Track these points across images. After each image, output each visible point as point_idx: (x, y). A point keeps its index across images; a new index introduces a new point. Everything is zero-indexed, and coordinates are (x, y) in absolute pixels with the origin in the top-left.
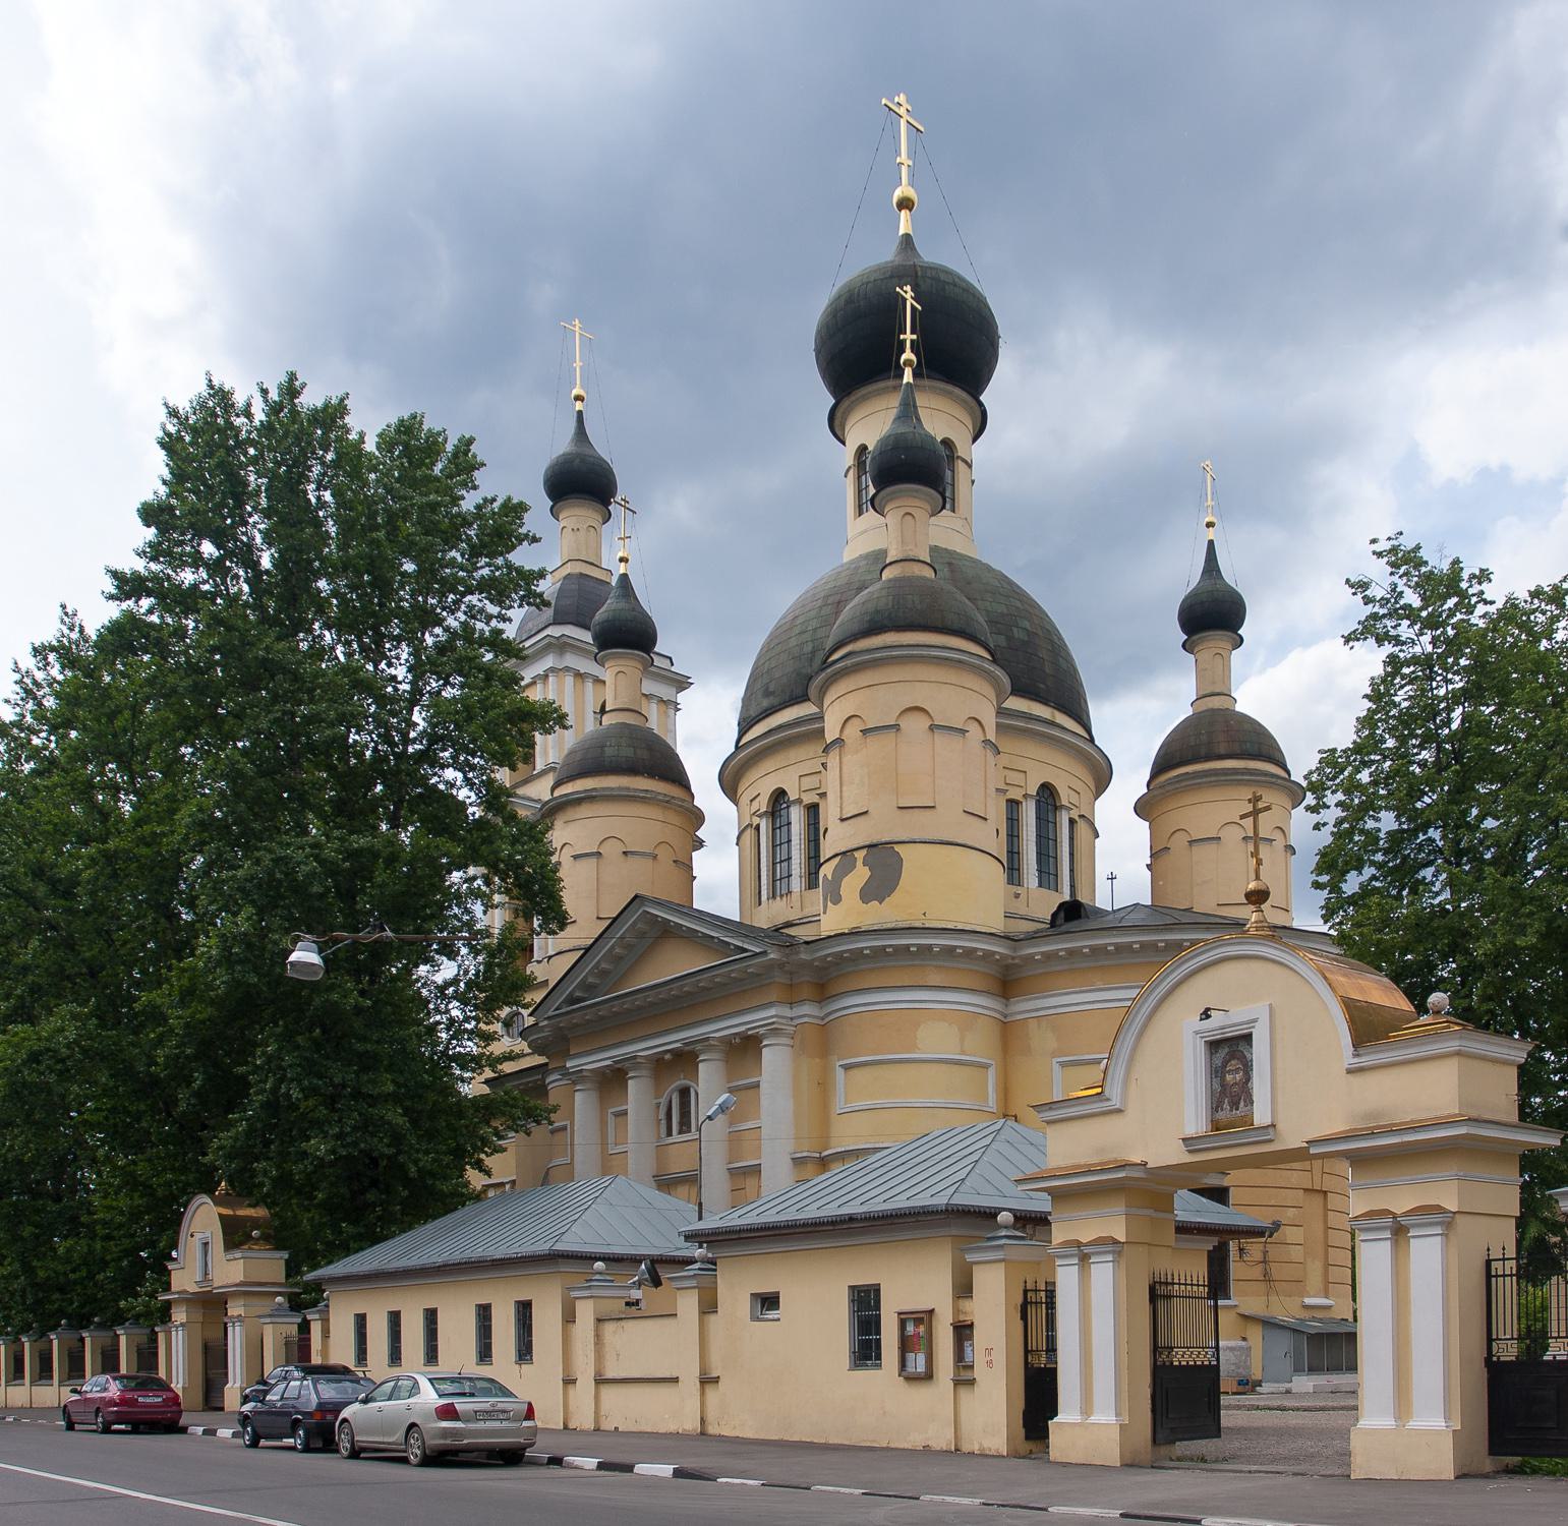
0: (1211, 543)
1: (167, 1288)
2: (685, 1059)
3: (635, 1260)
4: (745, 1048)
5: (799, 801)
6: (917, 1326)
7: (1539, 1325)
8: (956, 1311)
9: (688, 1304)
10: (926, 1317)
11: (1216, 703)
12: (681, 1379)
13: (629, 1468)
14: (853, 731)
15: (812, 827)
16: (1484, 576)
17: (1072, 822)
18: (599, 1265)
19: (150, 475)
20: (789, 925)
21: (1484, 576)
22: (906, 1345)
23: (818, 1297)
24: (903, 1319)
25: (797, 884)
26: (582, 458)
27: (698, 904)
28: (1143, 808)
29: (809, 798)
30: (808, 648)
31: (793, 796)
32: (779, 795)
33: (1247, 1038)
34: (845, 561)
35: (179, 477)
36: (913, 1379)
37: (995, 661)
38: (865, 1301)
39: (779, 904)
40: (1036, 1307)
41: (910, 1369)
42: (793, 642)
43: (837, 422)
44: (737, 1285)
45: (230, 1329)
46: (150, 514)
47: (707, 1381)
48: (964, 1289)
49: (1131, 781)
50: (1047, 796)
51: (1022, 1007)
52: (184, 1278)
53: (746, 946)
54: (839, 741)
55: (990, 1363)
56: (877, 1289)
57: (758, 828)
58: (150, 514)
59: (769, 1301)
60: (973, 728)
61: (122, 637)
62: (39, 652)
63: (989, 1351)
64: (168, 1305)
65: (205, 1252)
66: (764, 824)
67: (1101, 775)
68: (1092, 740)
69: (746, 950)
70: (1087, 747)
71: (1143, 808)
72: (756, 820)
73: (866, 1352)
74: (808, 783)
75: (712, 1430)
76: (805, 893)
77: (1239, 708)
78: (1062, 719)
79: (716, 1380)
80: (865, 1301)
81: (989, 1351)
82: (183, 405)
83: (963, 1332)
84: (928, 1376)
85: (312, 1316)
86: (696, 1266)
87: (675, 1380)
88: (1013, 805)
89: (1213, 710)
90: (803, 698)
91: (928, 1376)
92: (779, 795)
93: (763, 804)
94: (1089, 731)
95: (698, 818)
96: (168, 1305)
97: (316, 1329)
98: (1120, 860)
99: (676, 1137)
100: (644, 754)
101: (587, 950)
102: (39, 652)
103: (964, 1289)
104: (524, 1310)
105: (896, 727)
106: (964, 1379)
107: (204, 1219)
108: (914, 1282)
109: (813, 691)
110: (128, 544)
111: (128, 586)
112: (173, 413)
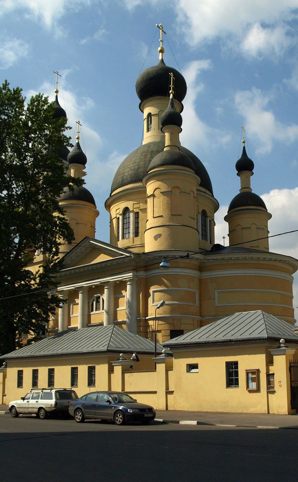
0: (244, 147)
2: (100, 289)
3: (132, 353)
4: (120, 286)
5: (133, 211)
6: (253, 375)
8: (268, 370)
11: (247, 190)
12: (20, 389)
13: (178, 422)
17: (210, 221)
20: (129, 247)
23: (214, 367)
25: (131, 235)
27: (96, 238)
28: (226, 219)
29: (136, 210)
30: (136, 167)
31: (131, 209)
34: (144, 143)
36: (251, 391)
37: (196, 174)
39: (125, 241)
41: (250, 388)
42: (131, 165)
43: (142, 104)
47: (168, 392)
48: (270, 362)
49: (223, 211)
51: (206, 275)
53: (124, 253)
55: (280, 386)
57: (119, 218)
60: (192, 193)
63: (280, 382)
66: (121, 217)
67: (216, 207)
68: (213, 196)
69: (123, 255)
70: (213, 199)
71: (226, 219)
72: (118, 216)
74: (135, 206)
76: (135, 238)
77: (253, 192)
78: (207, 192)
79: (172, 392)
81: (280, 382)
83: (270, 376)
84: (258, 390)
86: (164, 355)
87: (155, 392)
89: (246, 192)
90: (140, 180)
91: (258, 390)
94: (212, 194)
95: (97, 214)
98: (221, 233)
99: (94, 312)
101: (68, 252)
103: (270, 362)
104: (35, 373)
106: (271, 389)
108: (250, 362)
109: (144, 180)
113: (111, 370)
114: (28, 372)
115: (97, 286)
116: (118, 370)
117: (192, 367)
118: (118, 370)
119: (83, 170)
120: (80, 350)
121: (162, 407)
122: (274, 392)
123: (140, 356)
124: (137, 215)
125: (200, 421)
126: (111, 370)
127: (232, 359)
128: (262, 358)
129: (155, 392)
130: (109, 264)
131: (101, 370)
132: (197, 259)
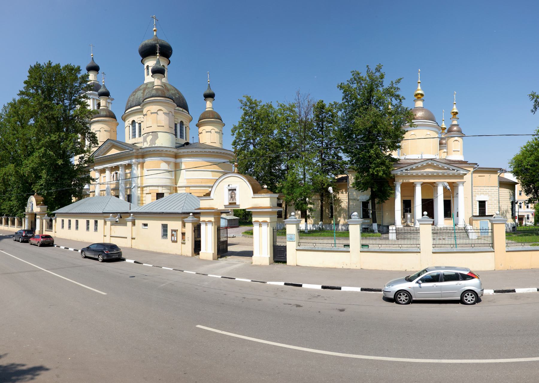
1: (25, 211)
7: (277, 191)
9: (129, 224)
10: (176, 231)
14: (149, 113)
15: (196, 231)
16: (261, 102)
18: (111, 215)
19: (25, 76)
21: (261, 102)
22: (172, 235)
23: (156, 225)
24: (172, 231)
26: (94, 64)
32: (133, 122)
33: (235, 190)
35: (31, 77)
38: (165, 227)
40: (197, 230)
44: (139, 222)
45: (38, 222)
46: (25, 82)
48: (184, 226)
50: (182, 123)
51: (178, 160)
52: (28, 209)
54: (146, 115)
56: (167, 225)
58: (25, 82)
59: (146, 225)
60: (170, 113)
61: (23, 102)
62: (8, 104)
64: (25, 215)
65: (33, 205)
73: (165, 235)
75: (133, 247)
78: (184, 110)
79: (134, 239)
80: (165, 227)
82: (33, 66)
83: (183, 234)
85: (53, 218)
87: (126, 238)
88: (176, 124)
90: (139, 105)
92: (133, 122)
93: (130, 122)
96: (25, 215)
97: (54, 221)
100: (108, 114)
102: (8, 104)
103: (184, 226)
105: (157, 113)
107: (32, 199)
108: (174, 225)
109: (141, 105)
110: (22, 87)
111: (22, 93)
112: (31, 67)
113: (105, 222)
114: (66, 221)
115: (115, 167)
116: (108, 223)
117: (146, 225)
118: (108, 223)
119: (145, 82)
120: (87, 211)
121: (129, 246)
122: (184, 243)
123: (122, 215)
124: (140, 124)
125: (137, 261)
126: (105, 222)
127: (165, 222)
128: (180, 223)
129: (126, 238)
130: (118, 155)
131: (101, 222)
132: (173, 152)
